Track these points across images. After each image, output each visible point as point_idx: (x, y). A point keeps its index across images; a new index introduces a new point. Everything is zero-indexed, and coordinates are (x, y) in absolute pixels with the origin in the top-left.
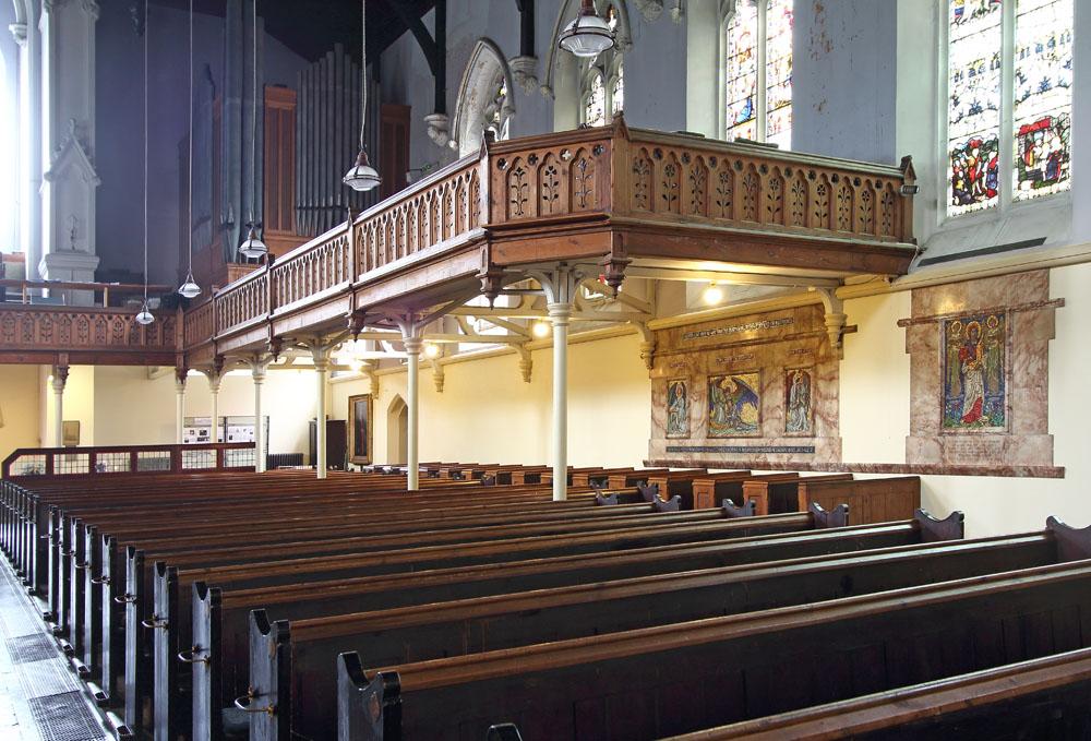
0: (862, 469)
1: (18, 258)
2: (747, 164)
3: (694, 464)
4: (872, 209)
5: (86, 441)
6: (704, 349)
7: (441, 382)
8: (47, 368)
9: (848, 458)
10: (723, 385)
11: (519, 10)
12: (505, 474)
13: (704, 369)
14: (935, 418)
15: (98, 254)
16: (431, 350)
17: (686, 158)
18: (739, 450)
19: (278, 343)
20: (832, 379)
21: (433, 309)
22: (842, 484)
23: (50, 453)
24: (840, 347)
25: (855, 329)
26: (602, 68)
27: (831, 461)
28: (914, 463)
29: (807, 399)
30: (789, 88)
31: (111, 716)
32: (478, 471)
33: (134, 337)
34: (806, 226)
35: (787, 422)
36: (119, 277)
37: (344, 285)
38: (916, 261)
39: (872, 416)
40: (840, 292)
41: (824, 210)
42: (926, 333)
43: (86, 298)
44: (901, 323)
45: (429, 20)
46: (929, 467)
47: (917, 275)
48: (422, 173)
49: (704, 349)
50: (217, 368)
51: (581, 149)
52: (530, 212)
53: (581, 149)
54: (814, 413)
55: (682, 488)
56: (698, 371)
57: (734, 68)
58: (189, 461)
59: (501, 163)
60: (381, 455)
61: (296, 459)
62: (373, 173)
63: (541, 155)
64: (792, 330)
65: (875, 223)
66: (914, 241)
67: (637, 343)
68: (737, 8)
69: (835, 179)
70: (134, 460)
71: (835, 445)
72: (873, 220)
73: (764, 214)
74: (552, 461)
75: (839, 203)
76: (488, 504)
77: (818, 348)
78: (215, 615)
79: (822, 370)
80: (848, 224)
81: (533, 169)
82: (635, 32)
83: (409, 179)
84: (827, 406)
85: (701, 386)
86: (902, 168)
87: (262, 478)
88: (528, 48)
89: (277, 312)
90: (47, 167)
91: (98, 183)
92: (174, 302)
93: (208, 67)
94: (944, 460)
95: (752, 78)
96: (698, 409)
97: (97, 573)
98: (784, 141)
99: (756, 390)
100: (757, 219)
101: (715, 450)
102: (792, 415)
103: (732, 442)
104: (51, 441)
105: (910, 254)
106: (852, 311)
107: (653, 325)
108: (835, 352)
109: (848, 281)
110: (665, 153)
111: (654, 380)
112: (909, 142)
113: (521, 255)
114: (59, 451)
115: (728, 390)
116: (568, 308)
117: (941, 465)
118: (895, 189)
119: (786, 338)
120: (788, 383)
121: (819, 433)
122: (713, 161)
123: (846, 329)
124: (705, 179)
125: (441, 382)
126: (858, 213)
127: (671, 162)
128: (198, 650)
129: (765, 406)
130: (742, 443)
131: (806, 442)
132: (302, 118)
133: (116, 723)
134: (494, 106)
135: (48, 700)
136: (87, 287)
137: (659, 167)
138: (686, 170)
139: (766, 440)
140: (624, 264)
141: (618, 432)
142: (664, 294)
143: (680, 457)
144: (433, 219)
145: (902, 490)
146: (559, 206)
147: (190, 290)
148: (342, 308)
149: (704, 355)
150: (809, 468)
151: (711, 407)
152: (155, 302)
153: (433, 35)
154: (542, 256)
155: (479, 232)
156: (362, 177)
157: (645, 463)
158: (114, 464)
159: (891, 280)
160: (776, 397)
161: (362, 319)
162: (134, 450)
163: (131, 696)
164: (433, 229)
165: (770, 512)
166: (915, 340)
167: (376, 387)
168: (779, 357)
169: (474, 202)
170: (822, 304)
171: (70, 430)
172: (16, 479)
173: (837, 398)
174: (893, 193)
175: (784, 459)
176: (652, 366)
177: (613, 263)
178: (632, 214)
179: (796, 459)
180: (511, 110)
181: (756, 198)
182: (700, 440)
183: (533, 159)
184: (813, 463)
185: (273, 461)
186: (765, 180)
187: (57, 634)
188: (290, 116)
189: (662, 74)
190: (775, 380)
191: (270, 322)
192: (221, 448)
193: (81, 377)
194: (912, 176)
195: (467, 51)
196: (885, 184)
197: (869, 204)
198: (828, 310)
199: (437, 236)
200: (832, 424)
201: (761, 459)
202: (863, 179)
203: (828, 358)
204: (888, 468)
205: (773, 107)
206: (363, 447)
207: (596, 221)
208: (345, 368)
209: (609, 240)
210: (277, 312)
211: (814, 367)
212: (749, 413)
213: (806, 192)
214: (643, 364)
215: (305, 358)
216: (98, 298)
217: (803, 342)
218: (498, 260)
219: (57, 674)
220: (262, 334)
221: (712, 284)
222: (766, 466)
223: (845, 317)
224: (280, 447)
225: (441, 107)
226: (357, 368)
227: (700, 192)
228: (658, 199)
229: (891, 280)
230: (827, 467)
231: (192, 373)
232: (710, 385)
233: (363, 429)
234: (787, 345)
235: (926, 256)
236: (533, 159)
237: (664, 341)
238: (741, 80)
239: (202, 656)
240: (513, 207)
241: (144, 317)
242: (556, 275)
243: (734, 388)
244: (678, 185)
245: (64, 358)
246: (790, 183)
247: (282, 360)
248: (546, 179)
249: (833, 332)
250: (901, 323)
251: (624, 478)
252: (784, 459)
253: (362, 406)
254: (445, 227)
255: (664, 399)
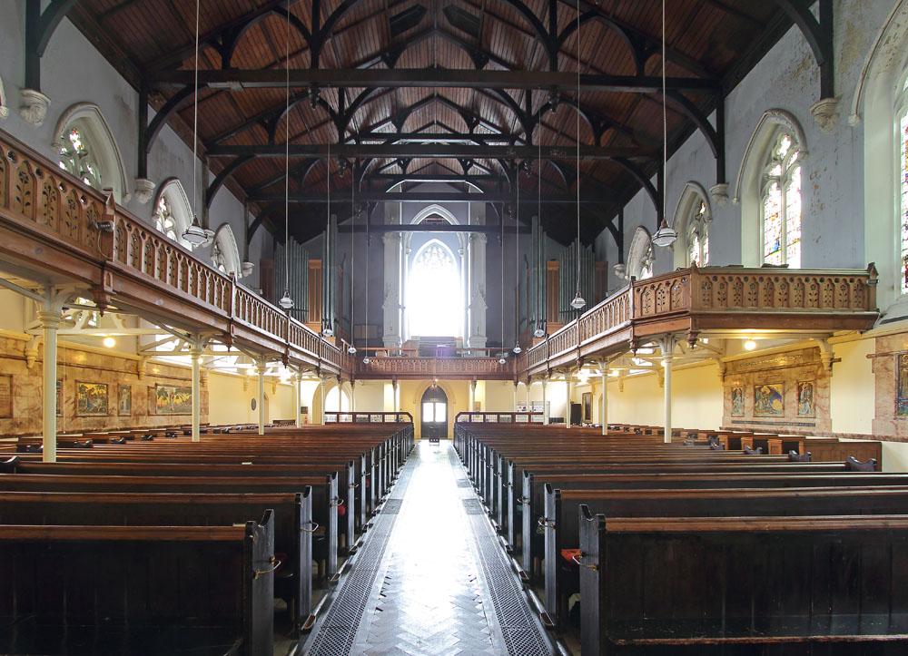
0: (844, 436)
1: (460, 339)
2: (772, 278)
3: (746, 430)
4: (848, 294)
5: (483, 410)
6: (751, 372)
7: (622, 388)
8: (470, 381)
9: (837, 429)
10: (762, 390)
11: (716, 157)
12: (648, 431)
13: (751, 382)
14: (892, 409)
15: (487, 336)
16: (615, 373)
17: (731, 279)
18: (772, 424)
19: (551, 371)
20: (825, 387)
21: (613, 356)
22: (832, 446)
23: (470, 414)
24: (830, 370)
25: (840, 360)
26: (698, 233)
27: (825, 431)
28: (877, 434)
29: (811, 396)
30: (800, 232)
31: (493, 521)
32: (637, 428)
33: (499, 369)
34: (803, 307)
35: (798, 410)
36: (493, 346)
37: (576, 346)
38: (878, 322)
39: (851, 408)
40: (830, 340)
41: (815, 298)
42: (885, 362)
43: (482, 354)
44: (868, 356)
45: (615, 221)
46: (887, 437)
47: (879, 329)
48: (613, 292)
49: (751, 372)
50: (529, 381)
51: (675, 281)
52: (652, 312)
53: (675, 281)
54: (815, 405)
55: (735, 443)
56: (748, 383)
57: (768, 224)
58: (519, 419)
59: (638, 290)
60: (596, 421)
61: (561, 420)
62: (583, 300)
63: (656, 285)
64: (802, 362)
65: (849, 302)
66: (878, 310)
67: (716, 370)
68: (770, 192)
69: (822, 281)
70: (498, 417)
71: (828, 423)
72: (848, 301)
73: (777, 302)
74: (663, 424)
75: (825, 293)
76: (637, 441)
77: (818, 370)
78: (514, 471)
79: (819, 382)
80: (831, 305)
81: (653, 292)
82: (714, 214)
83: (607, 295)
84: (821, 402)
85: (750, 390)
86: (869, 270)
87: (546, 427)
88: (721, 178)
89: (550, 358)
90: (469, 304)
91: (486, 307)
92: (513, 355)
93: (525, 256)
94: (898, 434)
95: (778, 228)
96: (749, 402)
97: (488, 464)
98: (795, 263)
99: (781, 393)
100: (773, 306)
101: (758, 423)
102: (802, 406)
103: (767, 420)
104: (471, 410)
105: (874, 318)
106: (838, 350)
107: (724, 360)
108: (828, 373)
109: (835, 334)
110: (719, 278)
111: (725, 387)
112: (873, 254)
113: (643, 331)
114: (474, 413)
115: (765, 392)
116: (671, 354)
117: (896, 436)
118: (863, 282)
119: (798, 366)
120: (800, 389)
121: (818, 416)
122: (746, 279)
123: (832, 361)
124: (742, 288)
125: (622, 388)
126: (838, 297)
127: (723, 282)
128: (525, 498)
129: (786, 400)
130: (773, 420)
131: (810, 421)
132: (561, 273)
133: (488, 510)
134: (646, 257)
135: (468, 500)
136: (483, 350)
137: (716, 285)
138: (731, 285)
139: (787, 418)
140: (697, 334)
141: (705, 412)
142: (730, 345)
143: (738, 426)
144: (611, 317)
145: (871, 450)
146: (665, 308)
147: (517, 350)
148: (574, 356)
149: (752, 374)
150: (812, 435)
151: (756, 401)
152: (506, 354)
153: (617, 227)
154: (657, 331)
155: (629, 322)
156: (578, 303)
157: (721, 428)
158: (492, 419)
159: (861, 333)
160: (792, 396)
161: (582, 360)
162: (498, 414)
163: (492, 502)
164: (611, 321)
165: (783, 453)
166: (877, 366)
167: (594, 388)
168: (794, 376)
169: (627, 308)
170: (583, 394)
171: (477, 405)
172: (460, 423)
173: (829, 397)
174: (862, 285)
175: (797, 429)
176: (724, 380)
177: (691, 333)
178: (701, 309)
179: (805, 429)
180: (653, 258)
181: (772, 295)
182: (749, 417)
183: (653, 287)
184: (814, 432)
185: (552, 420)
186: (777, 285)
187: (471, 479)
188: (557, 273)
189: (728, 236)
190: (792, 388)
191: (548, 362)
192: (530, 414)
193: (481, 385)
194: (876, 273)
195: (633, 232)
196: (856, 280)
197: (846, 292)
198: (823, 350)
199: (609, 322)
200: (826, 411)
201: (784, 428)
202: (841, 278)
203: (823, 376)
204: (860, 437)
205: (791, 242)
206: (588, 416)
207: (682, 314)
208: (580, 381)
209: (689, 323)
210: (550, 358)
211: (815, 381)
212: (776, 404)
213: (803, 289)
214: (719, 379)
215: (562, 377)
216: (487, 354)
217: (808, 367)
218: (637, 334)
219: (470, 492)
220: (545, 367)
221: (751, 340)
222: (787, 432)
223: (833, 354)
224: (554, 415)
225: (621, 261)
226: (584, 382)
227: (739, 295)
228: (715, 300)
229: (861, 333)
230: (823, 434)
231: (520, 383)
232: (755, 390)
233: (588, 408)
234: (799, 369)
235: (884, 318)
236: (653, 287)
237: (730, 368)
238: (773, 230)
239: (527, 501)
240: (644, 309)
241: (502, 361)
242: (665, 339)
243: (769, 391)
244: (726, 293)
245: (475, 378)
246: (792, 286)
247: (553, 378)
248: (659, 296)
249: (826, 362)
250: (868, 356)
251: (705, 435)
252: (797, 429)
253: (588, 398)
254: (615, 319)
255: (730, 397)
